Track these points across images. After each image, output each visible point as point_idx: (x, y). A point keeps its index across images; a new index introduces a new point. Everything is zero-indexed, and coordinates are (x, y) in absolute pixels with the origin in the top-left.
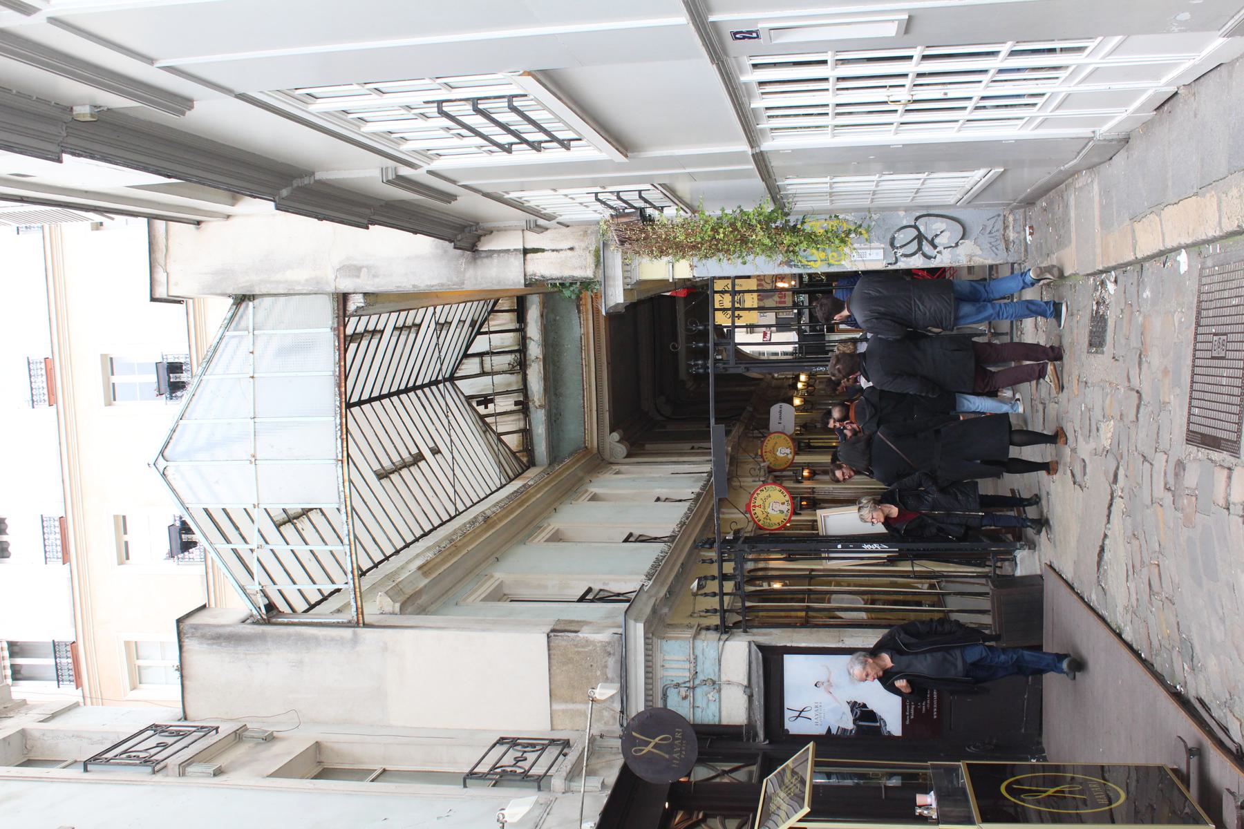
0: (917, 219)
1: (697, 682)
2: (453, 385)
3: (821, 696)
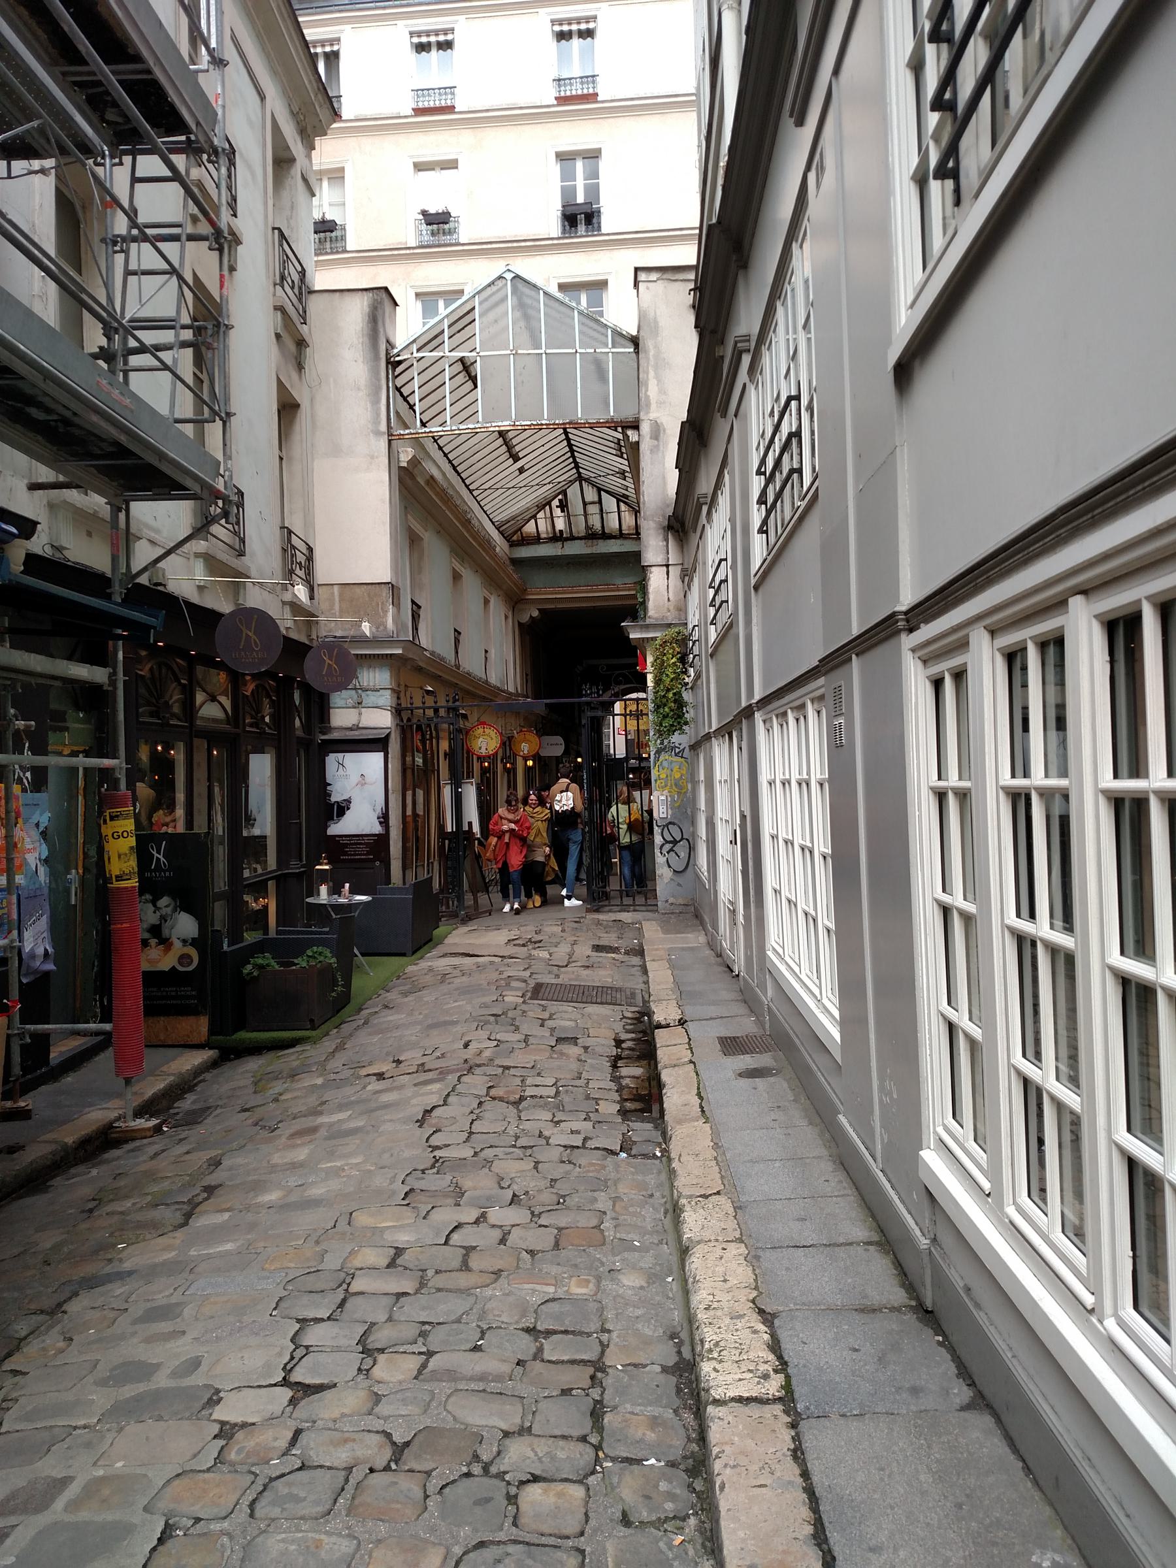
3: (354, 778)
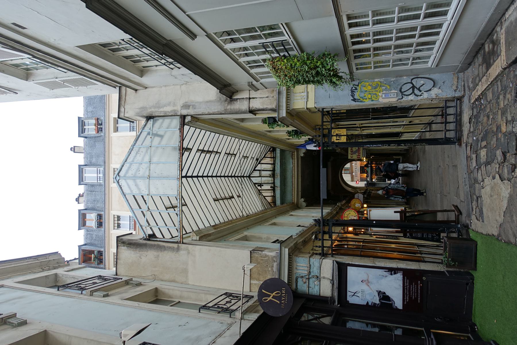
0: (412, 80)
1: (310, 276)
2: (250, 179)
3: (364, 287)
